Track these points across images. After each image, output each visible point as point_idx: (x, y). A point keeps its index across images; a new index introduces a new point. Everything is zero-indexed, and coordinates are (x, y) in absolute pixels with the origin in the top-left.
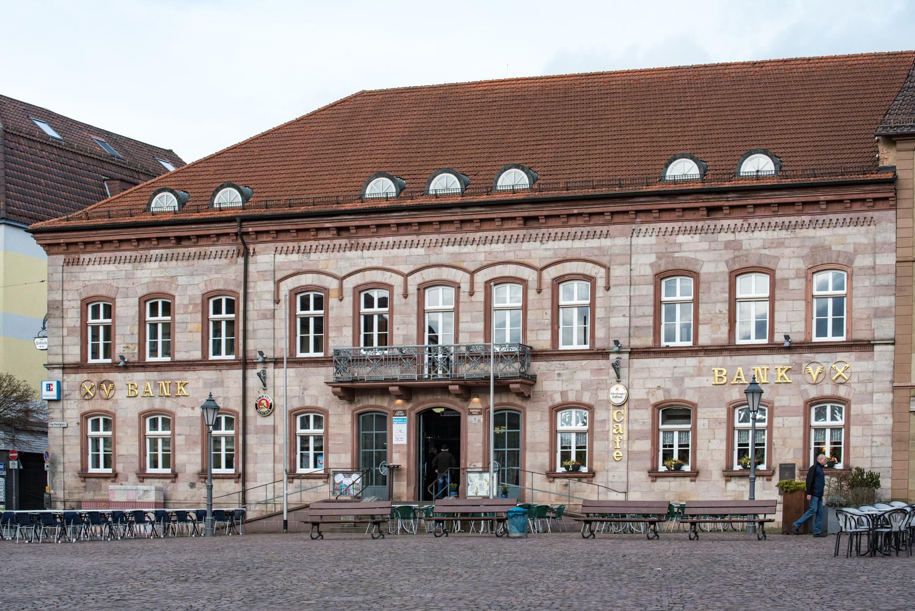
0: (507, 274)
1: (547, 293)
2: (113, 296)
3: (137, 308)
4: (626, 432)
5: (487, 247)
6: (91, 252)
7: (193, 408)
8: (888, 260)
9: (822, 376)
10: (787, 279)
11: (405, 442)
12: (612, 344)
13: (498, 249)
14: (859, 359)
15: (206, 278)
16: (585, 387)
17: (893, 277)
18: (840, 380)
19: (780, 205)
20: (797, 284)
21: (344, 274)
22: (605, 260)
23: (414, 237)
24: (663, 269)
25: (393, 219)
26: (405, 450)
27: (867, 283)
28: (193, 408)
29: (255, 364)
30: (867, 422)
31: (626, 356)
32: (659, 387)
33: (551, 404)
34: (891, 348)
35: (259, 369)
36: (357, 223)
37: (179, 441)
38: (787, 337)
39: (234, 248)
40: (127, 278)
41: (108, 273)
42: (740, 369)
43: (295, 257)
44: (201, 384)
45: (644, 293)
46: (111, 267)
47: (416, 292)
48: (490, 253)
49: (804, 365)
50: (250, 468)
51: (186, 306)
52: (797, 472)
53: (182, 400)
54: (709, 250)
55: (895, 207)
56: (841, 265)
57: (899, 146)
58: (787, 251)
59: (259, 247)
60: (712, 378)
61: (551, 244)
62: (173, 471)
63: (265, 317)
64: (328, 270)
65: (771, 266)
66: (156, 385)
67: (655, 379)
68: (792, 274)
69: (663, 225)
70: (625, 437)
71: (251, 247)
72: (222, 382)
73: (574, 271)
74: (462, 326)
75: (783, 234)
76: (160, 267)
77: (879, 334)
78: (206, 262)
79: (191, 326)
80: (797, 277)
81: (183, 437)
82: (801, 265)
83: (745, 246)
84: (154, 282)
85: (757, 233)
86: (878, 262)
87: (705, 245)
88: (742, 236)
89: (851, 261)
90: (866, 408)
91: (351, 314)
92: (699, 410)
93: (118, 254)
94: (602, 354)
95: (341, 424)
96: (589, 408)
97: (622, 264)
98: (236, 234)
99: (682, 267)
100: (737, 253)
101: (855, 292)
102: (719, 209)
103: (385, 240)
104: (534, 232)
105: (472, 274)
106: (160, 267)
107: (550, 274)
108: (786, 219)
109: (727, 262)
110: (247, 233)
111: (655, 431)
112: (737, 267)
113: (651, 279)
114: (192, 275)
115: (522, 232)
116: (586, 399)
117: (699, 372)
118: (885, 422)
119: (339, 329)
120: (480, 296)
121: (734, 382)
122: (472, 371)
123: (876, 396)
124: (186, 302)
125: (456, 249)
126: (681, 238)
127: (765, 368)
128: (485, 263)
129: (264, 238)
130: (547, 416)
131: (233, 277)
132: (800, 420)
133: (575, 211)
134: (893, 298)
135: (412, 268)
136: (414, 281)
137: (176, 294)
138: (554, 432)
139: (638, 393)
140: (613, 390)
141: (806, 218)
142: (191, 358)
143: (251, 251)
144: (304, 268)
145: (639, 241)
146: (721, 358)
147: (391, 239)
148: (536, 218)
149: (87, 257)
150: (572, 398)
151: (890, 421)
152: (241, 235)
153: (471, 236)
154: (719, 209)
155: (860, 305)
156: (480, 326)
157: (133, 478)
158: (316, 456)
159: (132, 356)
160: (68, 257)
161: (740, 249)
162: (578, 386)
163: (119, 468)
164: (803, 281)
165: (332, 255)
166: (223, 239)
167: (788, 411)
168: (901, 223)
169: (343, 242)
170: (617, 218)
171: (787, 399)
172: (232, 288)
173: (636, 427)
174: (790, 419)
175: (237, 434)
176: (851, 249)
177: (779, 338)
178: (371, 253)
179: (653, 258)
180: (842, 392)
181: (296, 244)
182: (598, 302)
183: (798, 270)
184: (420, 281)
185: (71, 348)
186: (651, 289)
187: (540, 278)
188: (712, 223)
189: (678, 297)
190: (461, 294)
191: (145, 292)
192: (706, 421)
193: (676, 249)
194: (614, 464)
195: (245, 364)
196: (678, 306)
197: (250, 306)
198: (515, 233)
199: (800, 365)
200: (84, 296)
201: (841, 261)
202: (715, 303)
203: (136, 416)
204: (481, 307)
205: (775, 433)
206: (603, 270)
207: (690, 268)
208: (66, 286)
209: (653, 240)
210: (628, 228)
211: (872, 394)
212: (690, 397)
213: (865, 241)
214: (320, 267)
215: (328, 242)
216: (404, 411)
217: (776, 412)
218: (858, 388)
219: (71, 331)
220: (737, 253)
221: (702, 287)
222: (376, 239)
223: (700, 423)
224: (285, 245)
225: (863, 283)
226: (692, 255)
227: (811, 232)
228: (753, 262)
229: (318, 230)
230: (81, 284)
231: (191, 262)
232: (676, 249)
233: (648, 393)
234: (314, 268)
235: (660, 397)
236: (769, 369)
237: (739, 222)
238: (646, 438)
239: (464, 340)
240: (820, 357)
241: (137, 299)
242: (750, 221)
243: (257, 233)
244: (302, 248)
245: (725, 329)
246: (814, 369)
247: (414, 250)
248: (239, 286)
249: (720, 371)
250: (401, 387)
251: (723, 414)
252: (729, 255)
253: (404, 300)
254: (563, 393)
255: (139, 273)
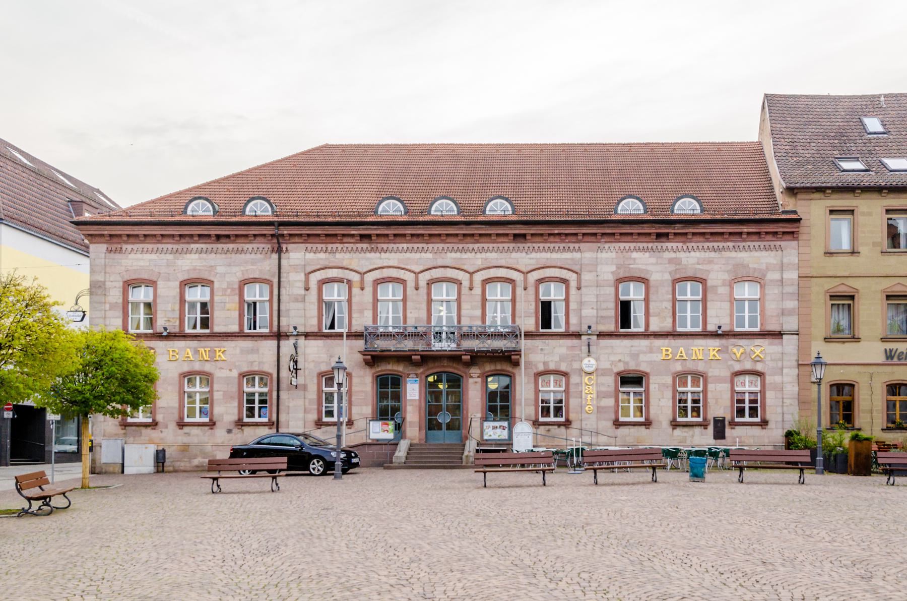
0: (499, 275)
1: (423, 290)
2: (154, 279)
3: (178, 290)
4: (595, 392)
5: (483, 255)
6: (133, 243)
7: (230, 370)
8: (792, 275)
9: (743, 356)
10: (716, 287)
11: (417, 397)
12: (292, 329)
13: (493, 257)
14: (770, 344)
15: (242, 268)
16: (563, 358)
17: (796, 287)
18: (758, 359)
19: (712, 234)
20: (723, 290)
21: (365, 270)
22: (576, 268)
23: (424, 245)
24: (621, 276)
25: (409, 231)
26: (417, 403)
27: (776, 291)
28: (230, 370)
29: (287, 336)
30: (780, 388)
31: (595, 337)
32: (620, 361)
33: (535, 371)
34: (796, 337)
35: (292, 341)
36: (378, 232)
37: (217, 396)
38: (165, 329)
39: (269, 246)
40: (168, 265)
41: (150, 260)
42: (682, 348)
43: (322, 256)
44: (238, 351)
45: (608, 292)
46: (153, 256)
47: (425, 285)
48: (486, 259)
49: (730, 347)
50: (283, 418)
51: (225, 290)
52: (727, 423)
53: (219, 364)
54: (657, 264)
55: (796, 239)
56: (757, 279)
57: (799, 196)
58: (716, 267)
59: (290, 246)
60: (659, 355)
61: (534, 255)
62: (211, 420)
63: (296, 300)
64: (351, 267)
65: (704, 277)
66: (196, 352)
67: (623, 354)
68: (720, 283)
69: (622, 245)
70: (595, 396)
71: (284, 247)
72: (258, 350)
73: (553, 275)
74: (463, 312)
75: (713, 254)
76: (200, 258)
77: (786, 327)
78: (243, 256)
79: (228, 306)
80: (724, 285)
81: (221, 393)
82: (726, 277)
83: (684, 262)
84: (195, 270)
85: (693, 254)
86: (785, 276)
87: (653, 260)
88: (682, 255)
89: (765, 276)
90: (778, 379)
91: (371, 301)
92: (651, 377)
93: (160, 246)
94: (575, 335)
95: (364, 384)
96: (565, 374)
97: (590, 272)
98: (272, 235)
99: (636, 275)
100: (678, 267)
101: (767, 297)
102: (666, 235)
103: (400, 246)
104: (521, 245)
105: (471, 274)
106: (200, 258)
107: (534, 276)
108: (716, 244)
109: (670, 273)
110: (283, 235)
111: (617, 392)
112: (678, 276)
113: (612, 282)
114: (230, 265)
115: (511, 245)
116: (563, 368)
117: (651, 351)
118: (792, 389)
119: (361, 312)
120: (478, 290)
121: (677, 358)
122: (481, 345)
123: (785, 371)
124: (225, 286)
125: (458, 255)
126: (635, 255)
127: (207, 349)
128: (482, 267)
129: (296, 239)
130: (532, 379)
131: (268, 268)
132: (728, 386)
133: (556, 232)
134: (796, 302)
135: (422, 268)
136: (424, 278)
137: (215, 280)
138: (537, 391)
139: (605, 365)
140: (586, 361)
141: (731, 244)
142: (229, 331)
143: (284, 249)
144: (331, 265)
145: (604, 255)
146: (667, 341)
147: (405, 246)
148: (524, 236)
149: (129, 247)
150: (552, 367)
151: (796, 389)
152: (278, 237)
153: (471, 246)
154: (666, 235)
155: (772, 307)
156: (479, 313)
157: (172, 426)
158: (260, 408)
159: (174, 328)
160: (110, 247)
161: (680, 264)
162: (557, 358)
163: (159, 418)
164: (728, 288)
165: (355, 255)
166: (258, 239)
167: (719, 380)
168: (802, 250)
169: (365, 246)
170: (586, 238)
171: (718, 372)
172: (267, 277)
173: (603, 389)
174: (720, 385)
175: (271, 391)
176: (764, 267)
177: (159, 329)
178: (387, 255)
179: (614, 268)
180: (759, 367)
181: (323, 246)
182: (572, 298)
183: (724, 280)
184: (429, 277)
185: (112, 320)
186: (612, 290)
187: (525, 280)
188: (659, 245)
189: (689, 297)
190: (463, 289)
191: (186, 277)
192: (656, 386)
193: (632, 262)
194: (587, 415)
195: (279, 336)
196: (747, 303)
197: (283, 291)
198: (506, 245)
199: (727, 347)
200: (126, 278)
201: (756, 275)
202: (662, 301)
203: (176, 375)
204: (479, 298)
205: (710, 395)
206: (575, 275)
207: (642, 276)
208: (108, 270)
209: (614, 255)
210: (595, 245)
211: (782, 369)
212: (644, 368)
213: (775, 262)
214: (345, 264)
215: (352, 245)
216: (416, 374)
217: (709, 380)
218: (771, 364)
219: (113, 307)
220: (678, 267)
221: (652, 291)
222: (393, 245)
223: (652, 387)
224: (314, 246)
225: (773, 292)
226: (644, 267)
227: (733, 254)
228: (690, 274)
229: (344, 235)
230: (123, 269)
231: (229, 255)
232: (632, 262)
233: (611, 365)
234: (340, 265)
235: (620, 368)
236: (703, 352)
237: (680, 245)
238: (611, 397)
239: (465, 322)
240: (743, 342)
241: (178, 283)
242: (688, 244)
243: (290, 235)
244: (329, 249)
245: (670, 320)
246: (738, 351)
247: (423, 255)
248: (273, 276)
249: (667, 350)
250: (422, 356)
251: (669, 380)
252: (672, 268)
253: (415, 292)
254: (545, 363)
255: (180, 262)
